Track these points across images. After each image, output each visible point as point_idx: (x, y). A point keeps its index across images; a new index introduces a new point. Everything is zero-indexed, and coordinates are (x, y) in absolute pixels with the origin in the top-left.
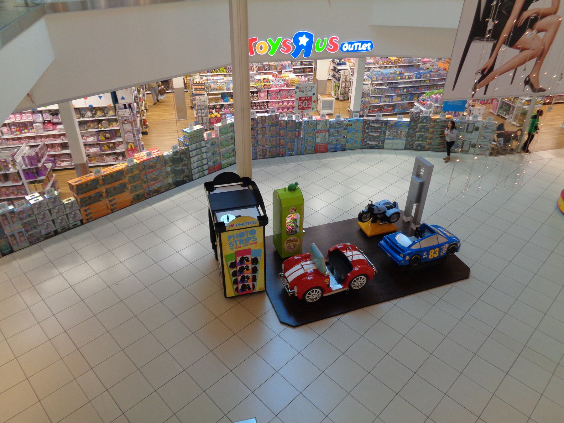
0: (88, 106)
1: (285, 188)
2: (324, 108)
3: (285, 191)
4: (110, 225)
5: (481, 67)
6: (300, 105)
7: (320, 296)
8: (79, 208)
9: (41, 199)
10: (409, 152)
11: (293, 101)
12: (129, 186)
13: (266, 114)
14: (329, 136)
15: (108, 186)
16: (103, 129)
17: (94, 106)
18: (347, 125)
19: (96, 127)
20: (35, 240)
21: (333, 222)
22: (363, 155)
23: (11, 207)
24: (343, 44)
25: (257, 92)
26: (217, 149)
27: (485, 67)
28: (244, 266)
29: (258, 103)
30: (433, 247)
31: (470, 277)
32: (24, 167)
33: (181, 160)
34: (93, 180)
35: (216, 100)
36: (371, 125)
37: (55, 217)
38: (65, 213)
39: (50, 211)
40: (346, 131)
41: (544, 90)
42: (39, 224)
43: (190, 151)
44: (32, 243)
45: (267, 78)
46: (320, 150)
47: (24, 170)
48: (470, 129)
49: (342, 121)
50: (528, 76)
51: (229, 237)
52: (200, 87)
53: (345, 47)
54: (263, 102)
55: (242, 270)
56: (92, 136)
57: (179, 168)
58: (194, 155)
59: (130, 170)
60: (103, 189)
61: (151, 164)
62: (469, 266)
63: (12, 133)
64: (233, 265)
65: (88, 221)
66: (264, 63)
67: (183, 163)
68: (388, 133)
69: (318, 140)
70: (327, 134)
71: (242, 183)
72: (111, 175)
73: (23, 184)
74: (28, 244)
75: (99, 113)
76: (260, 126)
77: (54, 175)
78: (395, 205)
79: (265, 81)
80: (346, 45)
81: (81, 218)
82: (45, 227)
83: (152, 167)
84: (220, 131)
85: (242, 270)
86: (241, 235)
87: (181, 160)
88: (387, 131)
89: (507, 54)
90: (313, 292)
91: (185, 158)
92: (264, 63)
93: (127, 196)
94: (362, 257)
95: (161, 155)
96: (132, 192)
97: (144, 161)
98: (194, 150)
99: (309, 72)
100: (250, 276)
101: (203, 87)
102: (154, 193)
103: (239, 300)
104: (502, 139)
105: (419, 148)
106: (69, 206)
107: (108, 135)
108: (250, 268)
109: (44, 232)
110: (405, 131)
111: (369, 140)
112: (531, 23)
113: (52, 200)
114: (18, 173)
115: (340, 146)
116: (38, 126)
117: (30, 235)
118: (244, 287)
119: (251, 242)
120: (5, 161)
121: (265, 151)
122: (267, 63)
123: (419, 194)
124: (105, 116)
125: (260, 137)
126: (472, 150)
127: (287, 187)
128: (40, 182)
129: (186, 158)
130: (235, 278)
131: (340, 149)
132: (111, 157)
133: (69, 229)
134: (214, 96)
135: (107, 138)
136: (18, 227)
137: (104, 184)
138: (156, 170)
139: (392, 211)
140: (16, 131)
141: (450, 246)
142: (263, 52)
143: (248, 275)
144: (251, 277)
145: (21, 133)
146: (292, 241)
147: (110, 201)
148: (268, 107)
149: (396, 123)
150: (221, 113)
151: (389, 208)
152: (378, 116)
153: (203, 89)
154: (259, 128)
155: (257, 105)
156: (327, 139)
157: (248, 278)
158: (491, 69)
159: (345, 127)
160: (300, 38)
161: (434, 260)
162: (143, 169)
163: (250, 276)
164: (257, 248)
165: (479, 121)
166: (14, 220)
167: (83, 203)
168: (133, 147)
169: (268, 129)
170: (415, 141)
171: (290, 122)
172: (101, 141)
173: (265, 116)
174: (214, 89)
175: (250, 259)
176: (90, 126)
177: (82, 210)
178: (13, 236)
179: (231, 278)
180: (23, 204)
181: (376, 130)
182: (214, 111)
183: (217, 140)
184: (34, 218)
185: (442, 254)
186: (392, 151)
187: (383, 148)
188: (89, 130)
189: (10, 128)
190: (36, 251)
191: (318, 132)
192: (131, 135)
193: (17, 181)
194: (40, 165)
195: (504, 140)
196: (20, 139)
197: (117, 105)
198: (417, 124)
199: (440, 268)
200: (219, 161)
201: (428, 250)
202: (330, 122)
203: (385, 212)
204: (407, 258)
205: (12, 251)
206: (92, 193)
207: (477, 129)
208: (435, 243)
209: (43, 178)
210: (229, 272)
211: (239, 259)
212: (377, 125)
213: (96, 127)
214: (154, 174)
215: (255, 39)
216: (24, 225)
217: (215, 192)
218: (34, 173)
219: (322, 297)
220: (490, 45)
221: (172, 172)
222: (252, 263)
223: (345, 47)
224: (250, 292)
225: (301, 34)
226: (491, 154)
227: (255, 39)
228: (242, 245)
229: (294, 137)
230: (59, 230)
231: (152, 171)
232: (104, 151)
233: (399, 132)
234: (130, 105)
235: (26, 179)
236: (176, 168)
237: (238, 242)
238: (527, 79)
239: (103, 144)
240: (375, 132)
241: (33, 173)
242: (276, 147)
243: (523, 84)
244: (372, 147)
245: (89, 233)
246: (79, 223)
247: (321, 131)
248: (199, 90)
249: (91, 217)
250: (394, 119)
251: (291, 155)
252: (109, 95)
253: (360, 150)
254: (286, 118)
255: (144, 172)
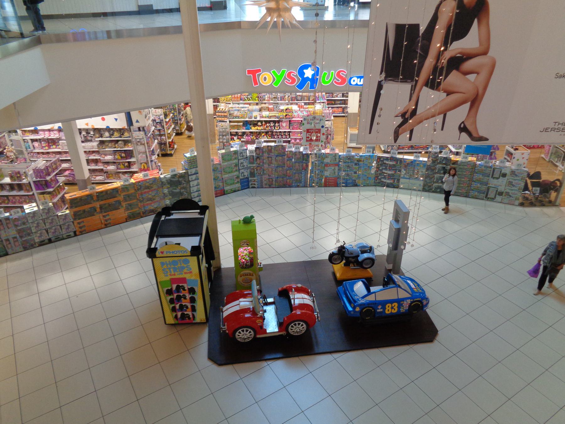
0: (105, 127)
1: (240, 220)
2: (351, 141)
3: (240, 223)
4: (99, 239)
5: (400, 109)
6: (308, 137)
7: (252, 336)
8: (72, 220)
9: (36, 209)
10: (426, 194)
11: (301, 133)
12: (124, 204)
13: (273, 144)
14: (339, 170)
15: (102, 202)
16: (119, 149)
17: (111, 127)
18: (359, 161)
19: (114, 146)
20: (28, 246)
21: (310, 260)
22: (375, 193)
23: (7, 214)
24: (351, 78)
25: (278, 122)
26: (220, 175)
27: (406, 110)
28: (181, 294)
29: (280, 132)
30: (391, 302)
31: (435, 342)
32: (34, 179)
33: (179, 183)
34: (87, 196)
35: (238, 127)
36: (385, 162)
37: (48, 226)
38: (59, 224)
39: (44, 220)
40: (357, 167)
41: (487, 139)
42: (33, 231)
43: (189, 175)
44: (25, 249)
45: (290, 108)
46: (332, 183)
47: (34, 182)
48: (496, 175)
49: (353, 156)
50: (463, 122)
51: (162, 264)
52: (223, 114)
53: (354, 81)
54: (285, 132)
55: (179, 298)
56: (109, 155)
57: (178, 190)
58: (194, 179)
59: (124, 188)
60: (97, 205)
61: (147, 184)
62: (438, 329)
63: (43, 147)
64: (169, 292)
65: (82, 233)
66: (298, 94)
67: (182, 186)
68: (403, 172)
69: (327, 174)
70: (337, 168)
71: (199, 211)
72: (106, 192)
73: (33, 194)
74: (22, 249)
75: (116, 134)
76: (266, 155)
77: (66, 188)
78: (371, 249)
79: (288, 111)
80: (355, 79)
81: (75, 230)
82: (38, 235)
83: (147, 187)
84: (222, 157)
85: (179, 298)
86: (174, 263)
87: (179, 183)
88: (403, 170)
89: (430, 98)
90: (243, 331)
91: (183, 182)
92: (298, 94)
93: (122, 213)
94: (311, 303)
95: (157, 176)
96: (127, 209)
97: (139, 182)
98: (194, 174)
99: (340, 104)
100: (189, 305)
101: (225, 114)
102: (150, 212)
103: (179, 328)
104: (538, 189)
105: (438, 190)
106: (63, 217)
107: (123, 155)
108: (188, 298)
109: (37, 240)
110: (422, 172)
111: (383, 178)
112: (456, 63)
113: (46, 211)
114: (29, 183)
115: (351, 181)
116: (63, 143)
117: (24, 241)
118: (183, 316)
119: (185, 270)
120: (19, 173)
121: (271, 180)
122: (301, 94)
123: (398, 239)
124: (120, 137)
125: (266, 166)
126: (499, 198)
127: (242, 218)
128: (49, 193)
129: (185, 181)
130: (173, 305)
131: (351, 185)
132: (126, 175)
133: (63, 239)
134: (236, 124)
135: (122, 157)
136: (12, 232)
137: (98, 200)
138: (152, 191)
139: (366, 255)
140: (45, 147)
141: (412, 303)
142: (268, 83)
143: (186, 304)
144: (189, 307)
145: (49, 148)
146: (246, 275)
147: (104, 216)
148: (290, 137)
149: (412, 162)
150: (242, 140)
151: (363, 252)
152: (393, 153)
153: (225, 116)
154: (265, 158)
155: (278, 134)
156: (337, 173)
157: (187, 307)
158: (414, 112)
159: (356, 162)
160: (305, 71)
161: (392, 316)
162: (138, 190)
163: (189, 305)
164: (193, 278)
165: (506, 167)
166: (9, 226)
167: (76, 216)
168: (146, 167)
169: (274, 159)
170: (434, 182)
171: (297, 153)
172: (117, 159)
173: (271, 146)
174: (236, 117)
175: (186, 288)
176: (108, 145)
177: (76, 222)
178: (8, 240)
179: (169, 305)
180: (18, 212)
181: (391, 167)
182: (235, 138)
183: (219, 166)
184: (28, 226)
185: (402, 310)
186: (409, 191)
187: (398, 187)
188: (106, 149)
189: (41, 143)
190: (27, 256)
191: (326, 165)
192: (144, 155)
193: (28, 191)
194: (48, 178)
195: (540, 190)
196: (48, 153)
197: (131, 127)
198: (436, 165)
199: (409, 325)
200: (221, 187)
201: (384, 303)
202: (340, 156)
203: (358, 256)
204: (358, 309)
205: (7, 254)
206: (87, 207)
207: (504, 175)
208: (395, 297)
209: (51, 190)
210: (166, 299)
211: (174, 286)
212: (391, 163)
213: (114, 146)
214: (151, 194)
215: (259, 71)
216: (19, 231)
217: (172, 217)
218: (43, 184)
219: (255, 338)
220: (407, 87)
221: (169, 194)
222: (190, 293)
223: (354, 81)
224: (189, 321)
225: (306, 67)
226: (522, 205)
227: (259, 71)
228: (176, 273)
229: (301, 168)
230: (53, 239)
231: (148, 192)
232: (120, 169)
233: (416, 172)
234: (143, 128)
235: (37, 190)
236: (175, 191)
237: (172, 269)
238: (462, 126)
239: (119, 163)
240: (390, 170)
241: (42, 185)
242: (283, 178)
243: (458, 132)
244: (388, 186)
245: (77, 245)
246: (72, 234)
247: (330, 165)
248: (221, 116)
249: (85, 230)
250: (411, 158)
251: (298, 186)
252: (122, 116)
253: (373, 188)
254: (293, 149)
255: (139, 192)
